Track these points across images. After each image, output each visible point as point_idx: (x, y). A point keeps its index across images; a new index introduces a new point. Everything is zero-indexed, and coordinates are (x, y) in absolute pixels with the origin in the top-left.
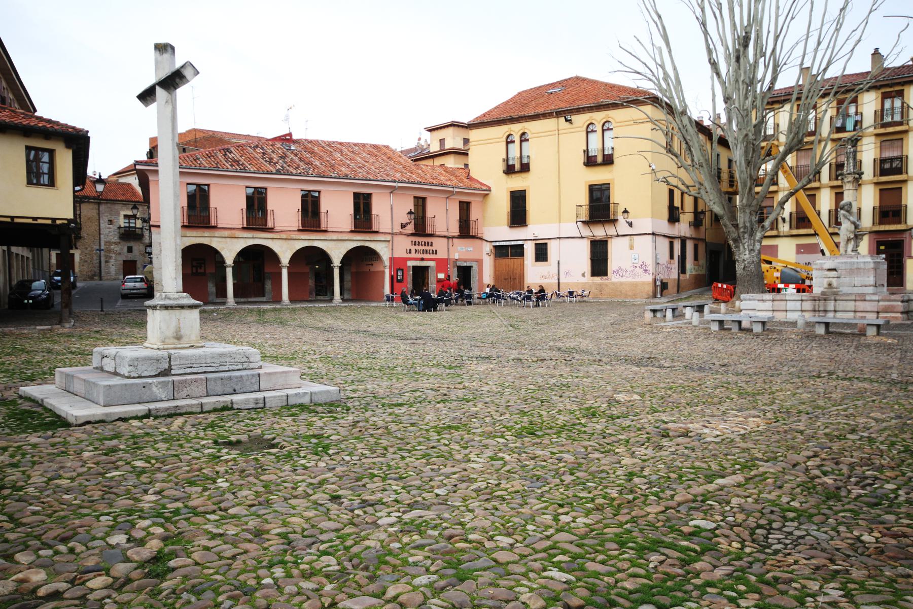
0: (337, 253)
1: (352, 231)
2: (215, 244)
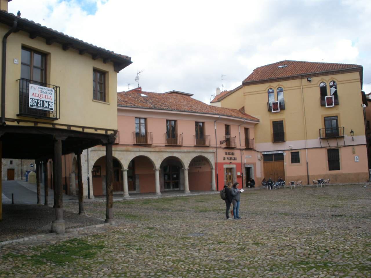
0: (186, 160)
1: (195, 146)
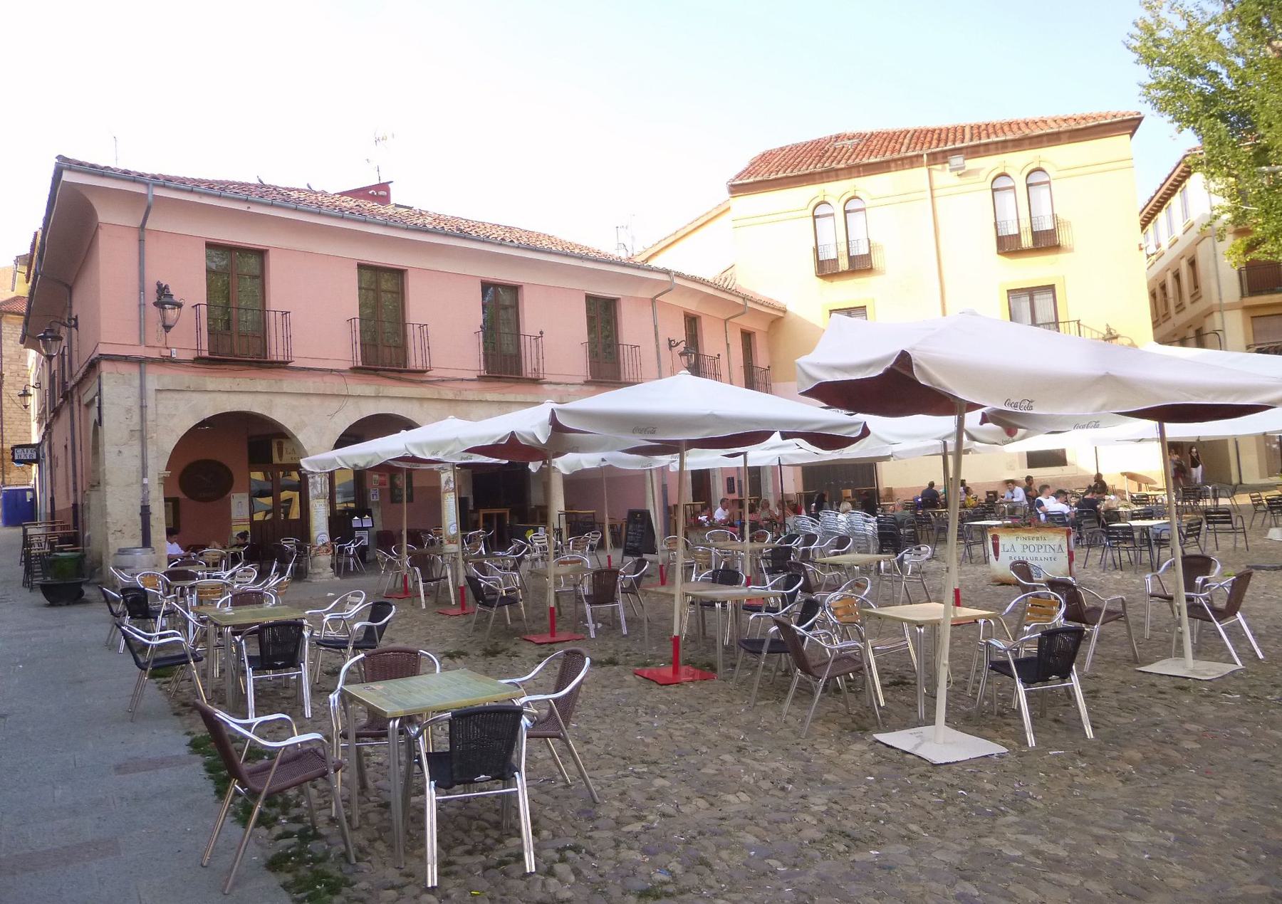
2: (281, 412)
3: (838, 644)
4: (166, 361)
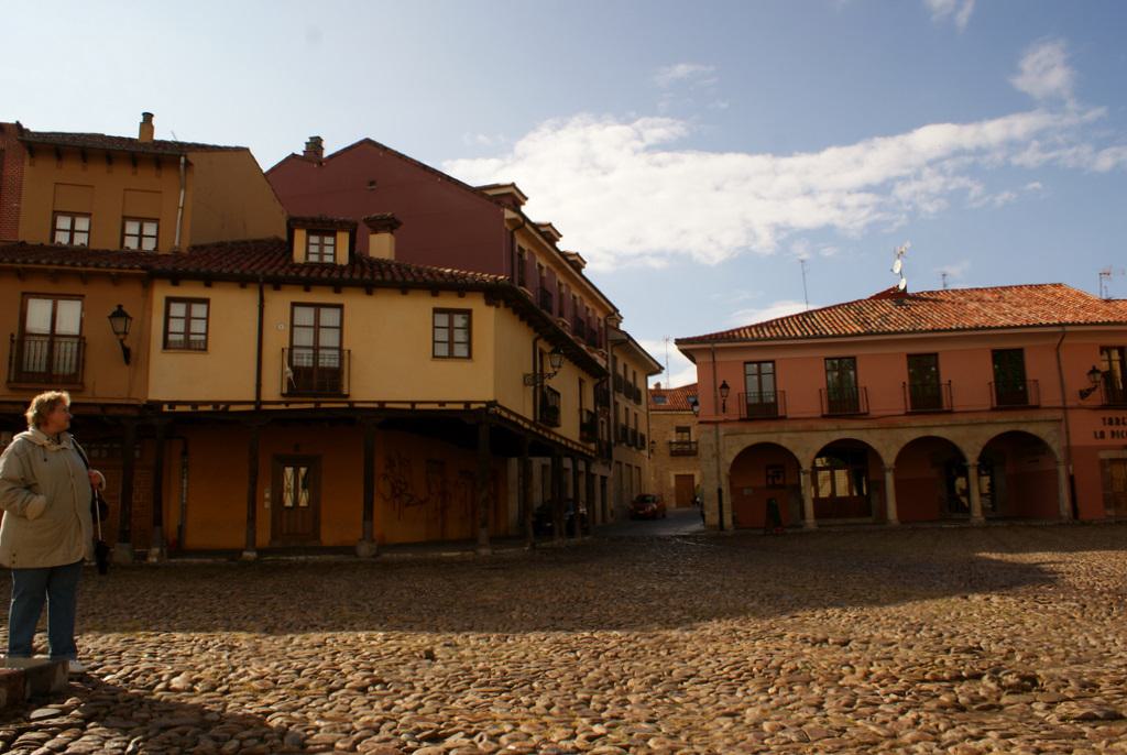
1: (993, 409)
2: (785, 440)
3: (555, 543)
4: (725, 422)
